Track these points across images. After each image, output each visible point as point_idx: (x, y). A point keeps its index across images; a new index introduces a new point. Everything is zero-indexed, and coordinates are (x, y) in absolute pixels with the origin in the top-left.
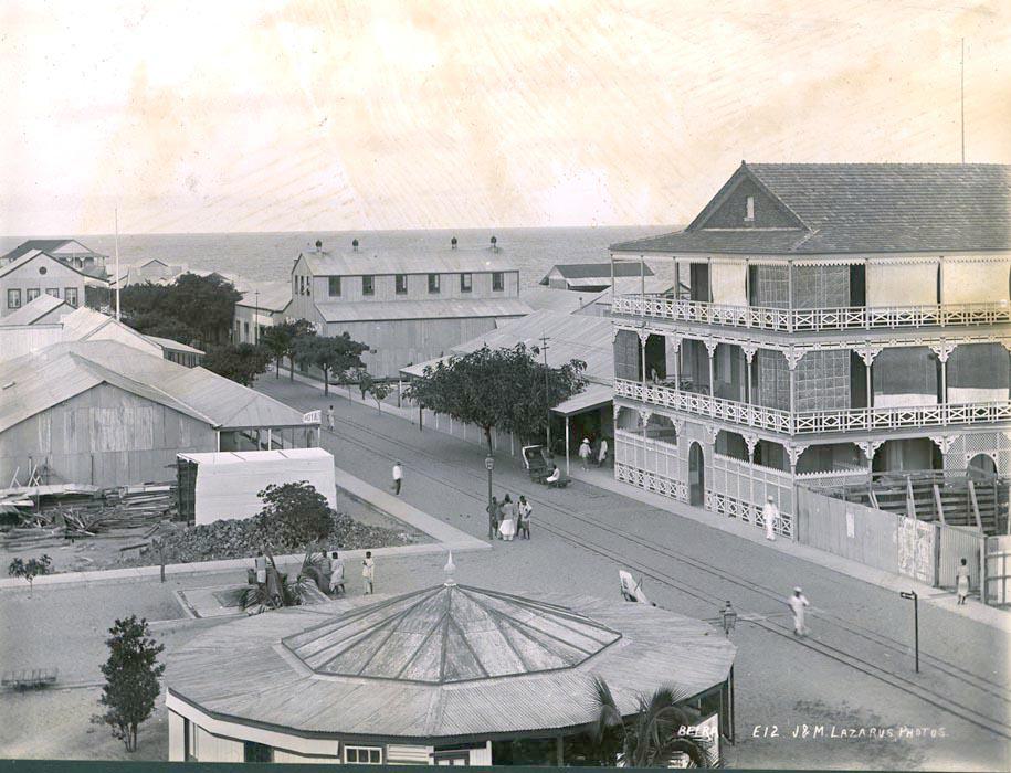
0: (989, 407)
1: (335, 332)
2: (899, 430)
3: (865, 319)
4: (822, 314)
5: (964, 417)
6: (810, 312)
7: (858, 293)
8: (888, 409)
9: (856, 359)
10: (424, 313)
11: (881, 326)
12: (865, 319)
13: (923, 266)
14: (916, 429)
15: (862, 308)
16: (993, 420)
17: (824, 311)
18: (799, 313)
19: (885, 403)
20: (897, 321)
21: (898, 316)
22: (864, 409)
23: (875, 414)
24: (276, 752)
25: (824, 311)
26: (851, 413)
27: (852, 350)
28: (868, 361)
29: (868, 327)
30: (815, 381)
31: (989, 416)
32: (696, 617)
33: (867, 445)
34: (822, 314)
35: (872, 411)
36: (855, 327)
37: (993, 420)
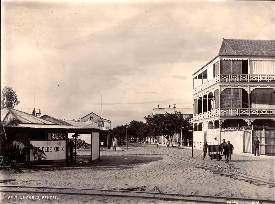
0: (267, 110)
1: (252, 184)
2: (261, 116)
3: (248, 78)
4: (231, 76)
5: (257, 113)
6: (227, 75)
7: (245, 70)
8: (257, 109)
9: (244, 92)
10: (145, 152)
11: (254, 81)
12: (248, 78)
13: (270, 61)
14: (268, 116)
15: (247, 74)
16: (259, 115)
17: (232, 75)
18: (223, 75)
19: (257, 107)
20: (260, 79)
21: (261, 78)
22: (247, 108)
23: (251, 110)
24: (90, 136)
25: (232, 75)
26: (242, 109)
27: (243, 88)
28: (248, 92)
29: (249, 81)
30: (229, 98)
31: (267, 114)
32: (147, 157)
33: (248, 120)
34: (231, 76)
35: (250, 109)
36: (244, 81)
37: (259, 115)
